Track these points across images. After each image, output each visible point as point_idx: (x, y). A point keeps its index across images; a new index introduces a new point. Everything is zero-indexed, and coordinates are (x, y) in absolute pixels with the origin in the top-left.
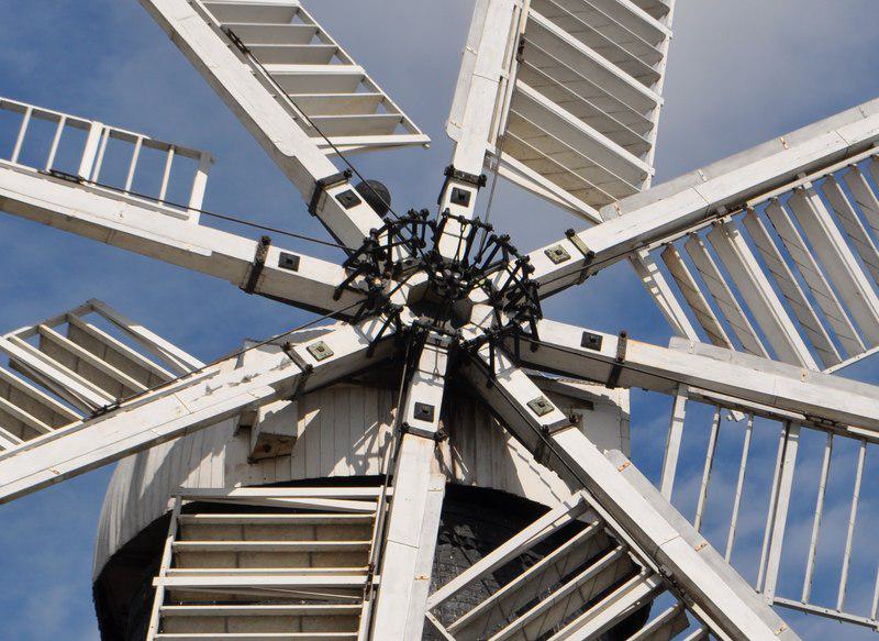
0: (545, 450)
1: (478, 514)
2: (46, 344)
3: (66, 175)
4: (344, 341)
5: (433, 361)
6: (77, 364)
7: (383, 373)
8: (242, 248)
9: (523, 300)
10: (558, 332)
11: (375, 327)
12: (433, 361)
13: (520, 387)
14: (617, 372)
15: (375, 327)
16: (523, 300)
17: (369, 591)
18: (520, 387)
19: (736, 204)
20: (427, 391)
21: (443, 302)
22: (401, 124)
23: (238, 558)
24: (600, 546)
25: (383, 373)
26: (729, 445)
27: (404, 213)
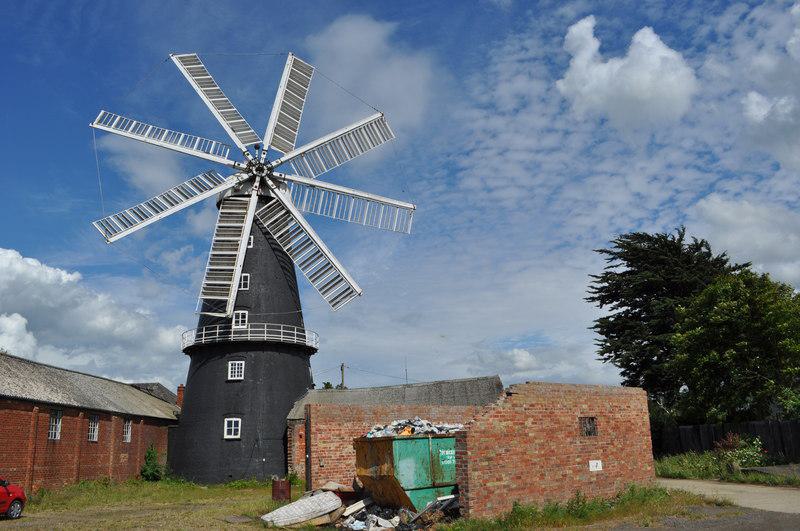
0: (273, 190)
1: (264, 199)
2: (192, 184)
3: (208, 153)
4: (245, 176)
5: (258, 179)
6: (210, 180)
7: (252, 180)
8: (232, 163)
9: (271, 169)
10: (276, 174)
11: (250, 174)
12: (258, 179)
13: (270, 183)
14: (284, 179)
15: (250, 174)
16: (271, 169)
17: (246, 213)
18: (270, 183)
19: (304, 153)
20: (257, 184)
21: (260, 170)
22: (199, 64)
23: (230, 208)
24: (280, 205)
25: (252, 180)
26: (299, 190)
27: (733, 265)
